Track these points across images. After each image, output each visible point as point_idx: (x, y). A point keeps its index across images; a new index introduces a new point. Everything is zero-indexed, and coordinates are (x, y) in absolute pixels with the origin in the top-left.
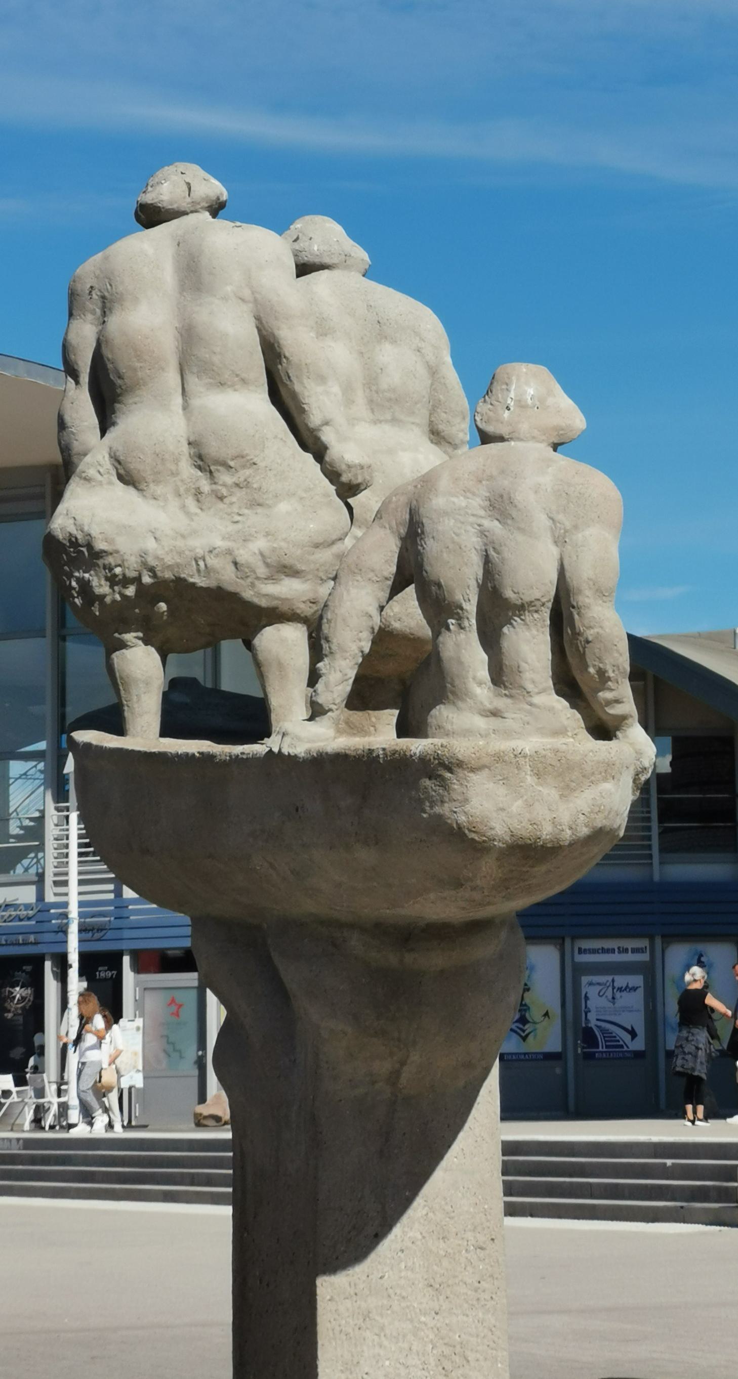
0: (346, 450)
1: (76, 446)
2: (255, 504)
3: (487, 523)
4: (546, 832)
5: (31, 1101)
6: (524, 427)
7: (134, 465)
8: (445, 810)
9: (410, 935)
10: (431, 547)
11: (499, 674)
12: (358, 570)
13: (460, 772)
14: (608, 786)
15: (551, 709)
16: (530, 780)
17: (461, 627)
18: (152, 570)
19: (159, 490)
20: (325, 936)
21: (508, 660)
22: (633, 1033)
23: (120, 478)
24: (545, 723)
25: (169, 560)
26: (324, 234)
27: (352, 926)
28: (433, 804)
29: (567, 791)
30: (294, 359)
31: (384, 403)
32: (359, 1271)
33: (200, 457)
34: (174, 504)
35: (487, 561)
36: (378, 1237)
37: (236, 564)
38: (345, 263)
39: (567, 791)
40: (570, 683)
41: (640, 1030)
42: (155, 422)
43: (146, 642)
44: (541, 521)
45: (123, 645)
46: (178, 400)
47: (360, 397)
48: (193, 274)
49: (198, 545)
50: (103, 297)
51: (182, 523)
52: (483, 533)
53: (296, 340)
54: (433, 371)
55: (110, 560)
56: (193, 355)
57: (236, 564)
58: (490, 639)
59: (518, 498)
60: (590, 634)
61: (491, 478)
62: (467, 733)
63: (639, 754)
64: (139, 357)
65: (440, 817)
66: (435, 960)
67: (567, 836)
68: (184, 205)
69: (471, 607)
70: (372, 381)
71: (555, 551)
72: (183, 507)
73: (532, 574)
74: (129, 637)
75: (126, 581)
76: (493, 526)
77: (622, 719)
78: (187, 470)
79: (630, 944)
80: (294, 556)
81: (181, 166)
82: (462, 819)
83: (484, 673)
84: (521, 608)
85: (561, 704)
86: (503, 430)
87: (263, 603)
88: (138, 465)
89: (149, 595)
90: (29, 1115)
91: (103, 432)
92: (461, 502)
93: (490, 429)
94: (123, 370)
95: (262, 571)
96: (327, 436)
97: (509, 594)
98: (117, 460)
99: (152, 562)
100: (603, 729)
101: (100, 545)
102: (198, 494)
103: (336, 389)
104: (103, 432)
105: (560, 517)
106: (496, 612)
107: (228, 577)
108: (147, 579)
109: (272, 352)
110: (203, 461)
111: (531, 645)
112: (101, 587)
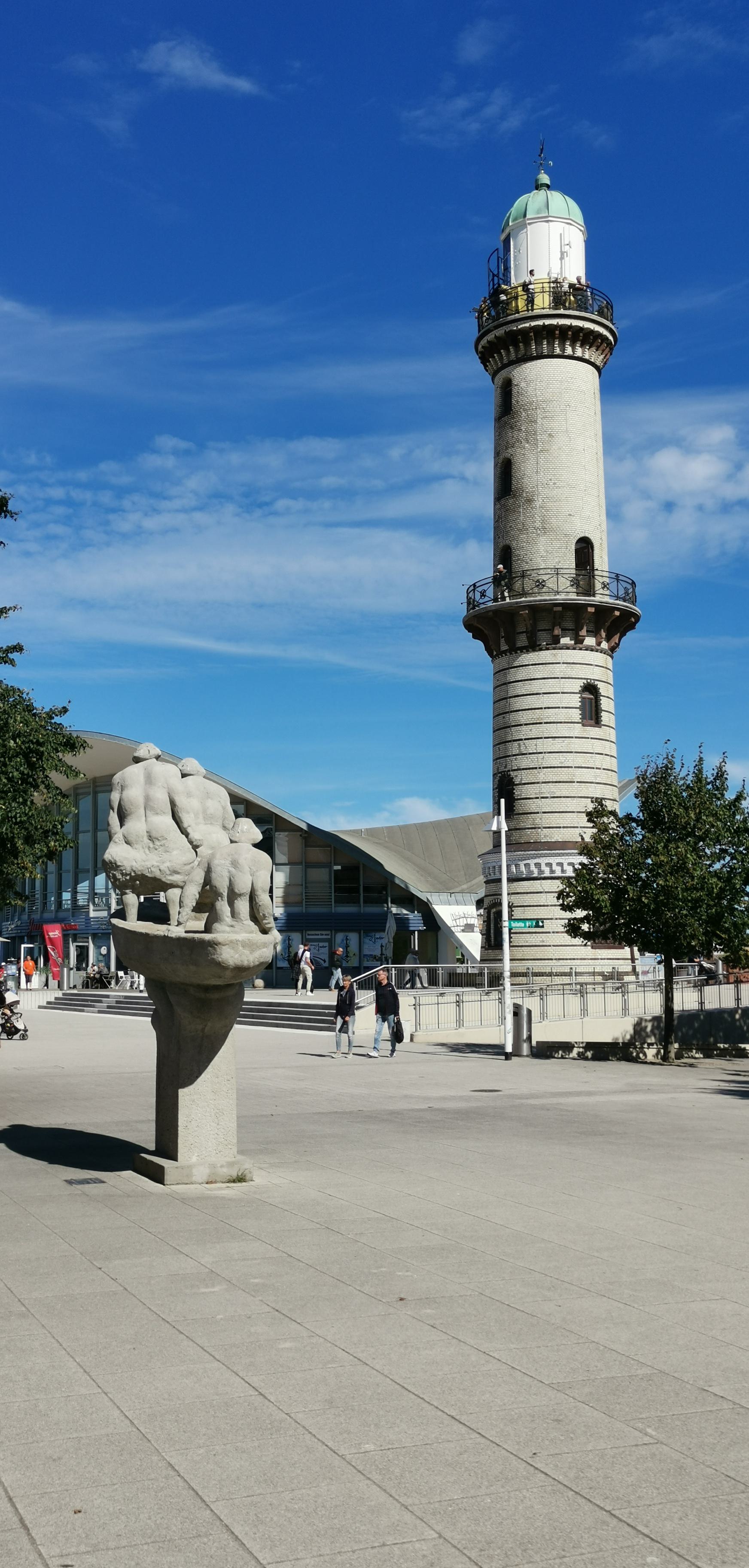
0: (195, 835)
1: (113, 831)
2: (166, 851)
4: (246, 963)
5: (130, 980)
6: (243, 839)
7: (130, 839)
8: (215, 957)
9: (207, 989)
10: (214, 876)
11: (234, 914)
12: (191, 881)
14: (265, 950)
16: (241, 948)
20: (183, 988)
21: (236, 910)
22: (325, 961)
24: (248, 931)
26: (191, 764)
29: (252, 951)
31: (209, 819)
34: (142, 851)
35: (230, 880)
36: (197, 1077)
38: (198, 774)
39: (252, 952)
40: (255, 917)
41: (327, 960)
42: (136, 825)
44: (247, 869)
45: (126, 894)
46: (144, 818)
47: (201, 816)
48: (149, 779)
49: (149, 864)
52: (229, 872)
53: (180, 801)
54: (224, 808)
58: (231, 903)
59: (240, 861)
60: (260, 903)
62: (224, 932)
63: (275, 939)
66: (215, 996)
67: (252, 965)
68: (147, 757)
69: (225, 894)
70: (204, 811)
71: (251, 878)
73: (243, 885)
74: (127, 891)
75: (126, 875)
76: (232, 869)
77: (270, 928)
79: (324, 932)
80: (178, 869)
81: (147, 744)
83: (229, 914)
84: (240, 895)
88: (131, 839)
89: (133, 879)
90: (129, 984)
91: (121, 827)
93: (233, 839)
95: (168, 872)
96: (189, 830)
97: (236, 891)
98: (125, 837)
100: (264, 931)
101: (119, 864)
103: (192, 815)
104: (121, 827)
106: (233, 896)
107: (158, 874)
108: (133, 874)
109: (173, 804)
110: (151, 838)
111: (243, 906)
112: (119, 876)
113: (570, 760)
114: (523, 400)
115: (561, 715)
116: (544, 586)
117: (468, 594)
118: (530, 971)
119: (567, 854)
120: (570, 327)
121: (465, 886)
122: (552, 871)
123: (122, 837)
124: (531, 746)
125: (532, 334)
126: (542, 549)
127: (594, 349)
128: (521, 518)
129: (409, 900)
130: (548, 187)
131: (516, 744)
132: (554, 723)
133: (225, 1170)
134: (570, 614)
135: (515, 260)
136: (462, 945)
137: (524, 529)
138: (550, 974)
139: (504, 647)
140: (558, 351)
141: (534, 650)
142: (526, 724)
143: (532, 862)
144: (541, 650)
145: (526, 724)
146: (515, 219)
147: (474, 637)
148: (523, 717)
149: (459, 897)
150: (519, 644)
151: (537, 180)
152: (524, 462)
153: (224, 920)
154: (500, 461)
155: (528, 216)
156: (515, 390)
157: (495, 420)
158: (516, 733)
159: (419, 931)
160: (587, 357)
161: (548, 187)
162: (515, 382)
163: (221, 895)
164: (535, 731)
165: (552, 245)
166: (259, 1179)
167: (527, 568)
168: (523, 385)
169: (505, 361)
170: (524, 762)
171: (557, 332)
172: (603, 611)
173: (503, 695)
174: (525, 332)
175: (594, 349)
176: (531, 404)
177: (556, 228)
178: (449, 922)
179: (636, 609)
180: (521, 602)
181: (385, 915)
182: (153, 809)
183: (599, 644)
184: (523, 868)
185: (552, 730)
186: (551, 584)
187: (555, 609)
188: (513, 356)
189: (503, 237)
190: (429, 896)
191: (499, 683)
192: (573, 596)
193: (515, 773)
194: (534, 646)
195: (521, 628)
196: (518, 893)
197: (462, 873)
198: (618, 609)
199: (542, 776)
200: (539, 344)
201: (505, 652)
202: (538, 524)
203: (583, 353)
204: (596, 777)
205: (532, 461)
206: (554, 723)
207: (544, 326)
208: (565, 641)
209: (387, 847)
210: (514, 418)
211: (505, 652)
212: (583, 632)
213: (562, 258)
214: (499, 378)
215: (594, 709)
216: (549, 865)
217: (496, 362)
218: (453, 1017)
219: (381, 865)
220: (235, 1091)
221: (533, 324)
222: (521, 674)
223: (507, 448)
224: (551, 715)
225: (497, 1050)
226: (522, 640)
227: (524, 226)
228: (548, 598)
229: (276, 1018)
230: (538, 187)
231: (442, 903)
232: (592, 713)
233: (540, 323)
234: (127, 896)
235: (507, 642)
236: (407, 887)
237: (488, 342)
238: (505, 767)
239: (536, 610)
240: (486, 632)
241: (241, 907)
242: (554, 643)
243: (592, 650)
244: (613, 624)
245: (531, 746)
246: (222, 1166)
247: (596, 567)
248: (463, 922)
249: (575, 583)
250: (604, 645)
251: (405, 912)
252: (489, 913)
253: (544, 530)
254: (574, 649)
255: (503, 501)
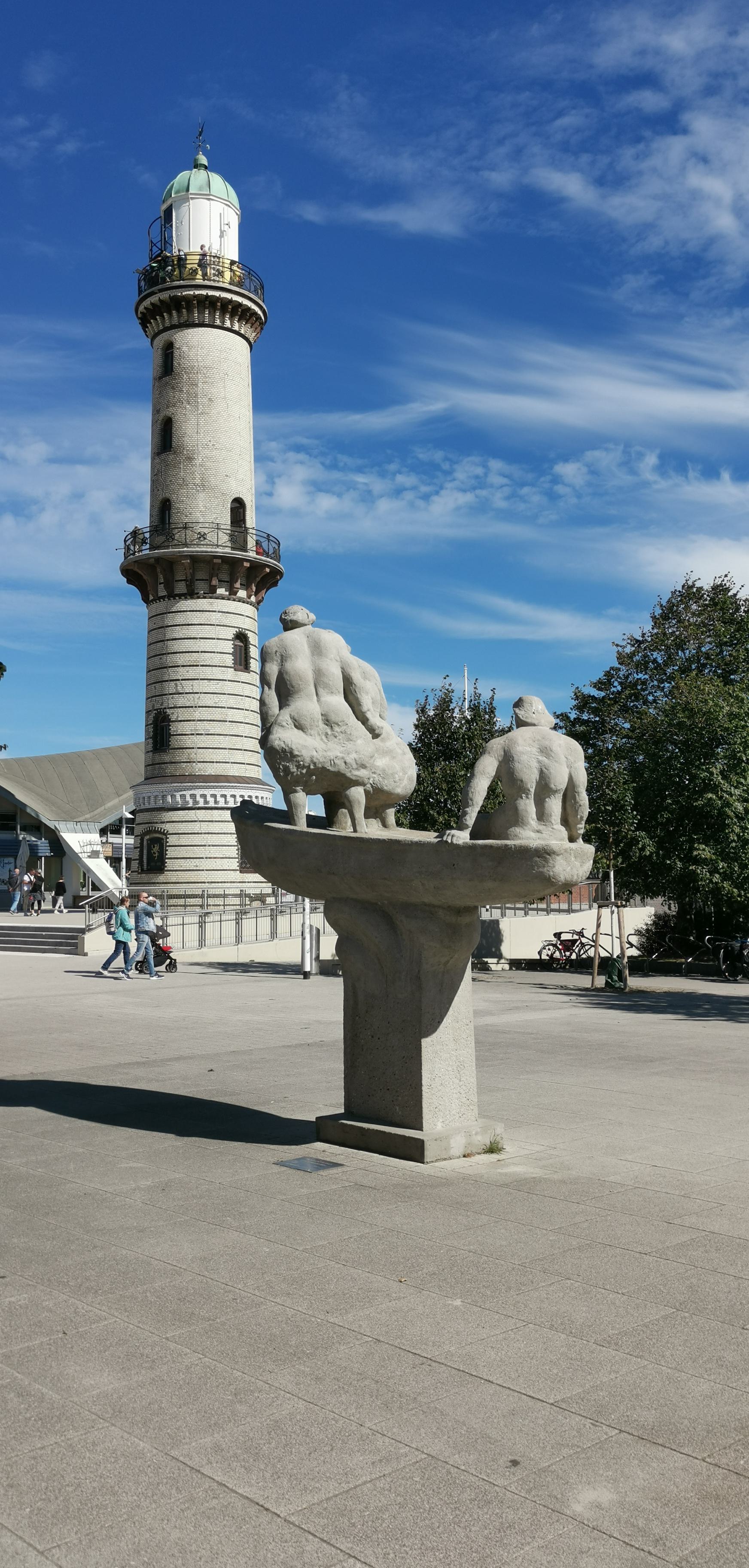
2: (349, 740)
3: (540, 758)
6: (543, 721)
7: (303, 722)
13: (553, 856)
15: (560, 831)
16: (573, 859)
17: (527, 797)
18: (315, 764)
19: (312, 732)
23: (296, 726)
25: (321, 760)
27: (439, 907)
28: (539, 867)
30: (358, 685)
32: (434, 1036)
33: (327, 720)
35: (541, 772)
37: (345, 763)
42: (307, 705)
43: (303, 791)
45: (296, 791)
46: (315, 697)
48: (317, 649)
49: (331, 755)
50: (282, 656)
51: (324, 746)
52: (539, 762)
55: (299, 759)
56: (320, 680)
57: (345, 763)
58: (540, 803)
59: (554, 749)
61: (538, 740)
62: (528, 838)
64: (301, 680)
65: (542, 872)
68: (306, 622)
69: (532, 790)
72: (322, 739)
74: (298, 788)
75: (304, 767)
77: (467, 827)
78: (322, 725)
82: (551, 873)
85: (563, 829)
86: (535, 722)
87: (354, 778)
89: (310, 773)
92: (528, 749)
94: (294, 684)
95: (355, 766)
96: (369, 715)
97: (552, 786)
98: (294, 719)
99: (315, 760)
101: (296, 753)
102: (326, 734)
105: (569, 757)
107: (342, 767)
108: (312, 767)
110: (328, 722)
111: (555, 805)
112: (293, 769)
113: (224, 701)
114: (185, 363)
115: (216, 659)
116: (205, 539)
117: (125, 541)
118: (165, 894)
119: (221, 787)
120: (231, 301)
121: (88, 816)
122: (206, 802)
123: (290, 721)
124: (188, 686)
125: (195, 302)
126: (201, 504)
127: (249, 325)
128: (182, 474)
129: (37, 827)
130: (206, 167)
131: (173, 684)
132: (209, 666)
133: (479, 1138)
134: (226, 567)
135: (176, 231)
136: (89, 870)
137: (185, 484)
138: (186, 896)
139: (162, 592)
140: (218, 322)
141: (192, 598)
142: (183, 666)
143: (188, 793)
144: (199, 598)
145: (183, 666)
146: (177, 192)
147: (129, 582)
148: (181, 659)
149: (84, 825)
150: (177, 591)
151: (196, 160)
152: (185, 422)
153: (528, 823)
154: (161, 418)
155: (191, 191)
156: (176, 353)
157: (155, 379)
158: (172, 674)
159: (46, 857)
160: (242, 332)
161: (206, 167)
162: (177, 345)
163: (526, 791)
164: (192, 673)
165: (210, 223)
166: (510, 1149)
167: (186, 520)
168: (185, 349)
169: (161, 327)
170: (181, 701)
171: (219, 304)
172: (256, 566)
173: (160, 637)
174: (188, 300)
175: (249, 325)
176: (193, 368)
177: (217, 207)
178: (77, 849)
179: (281, 566)
180: (183, 552)
181: (17, 843)
182: (327, 686)
183: (249, 597)
184: (178, 799)
185: (208, 672)
186: (211, 537)
187: (215, 561)
188: (175, 320)
189: (164, 207)
190: (56, 824)
191: (155, 626)
192: (228, 550)
193: (172, 711)
194: (191, 594)
195: (180, 575)
196: (173, 822)
197: (84, 803)
198: (269, 566)
199: (198, 714)
200: (201, 313)
201: (163, 597)
202: (198, 481)
203: (240, 327)
204: (245, 717)
205: (193, 421)
206: (209, 666)
207: (207, 296)
208: (221, 591)
209: (7, 778)
210: (175, 379)
211: (163, 597)
212: (238, 585)
213: (221, 236)
214: (160, 341)
215: (243, 656)
216: (204, 796)
217: (157, 324)
218: (196, 937)
219: (13, 795)
220: (473, 1038)
221: (197, 292)
222: (179, 619)
223: (168, 407)
224: (207, 659)
225: (297, 970)
226: (181, 588)
227: (187, 199)
228: (209, 550)
229: (16, 942)
230: (197, 166)
231: (69, 831)
232: (242, 661)
233: (204, 292)
234: (297, 795)
235: (166, 588)
236: (38, 816)
237: (152, 304)
238: (162, 704)
239: (195, 559)
240: (145, 577)
241: (554, 807)
242: (211, 592)
243: (244, 602)
244: (260, 578)
245: (188, 686)
246: (476, 1134)
247: (248, 526)
248: (89, 849)
249: (233, 538)
250: (253, 599)
251: (34, 839)
252: (142, 840)
253: (203, 486)
254: (229, 599)
255: (163, 456)
